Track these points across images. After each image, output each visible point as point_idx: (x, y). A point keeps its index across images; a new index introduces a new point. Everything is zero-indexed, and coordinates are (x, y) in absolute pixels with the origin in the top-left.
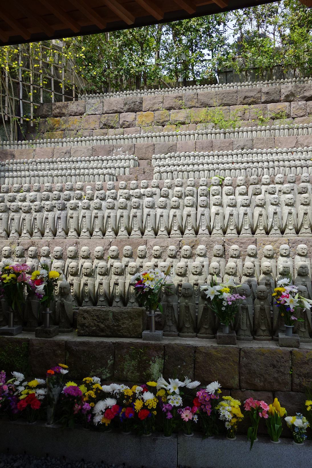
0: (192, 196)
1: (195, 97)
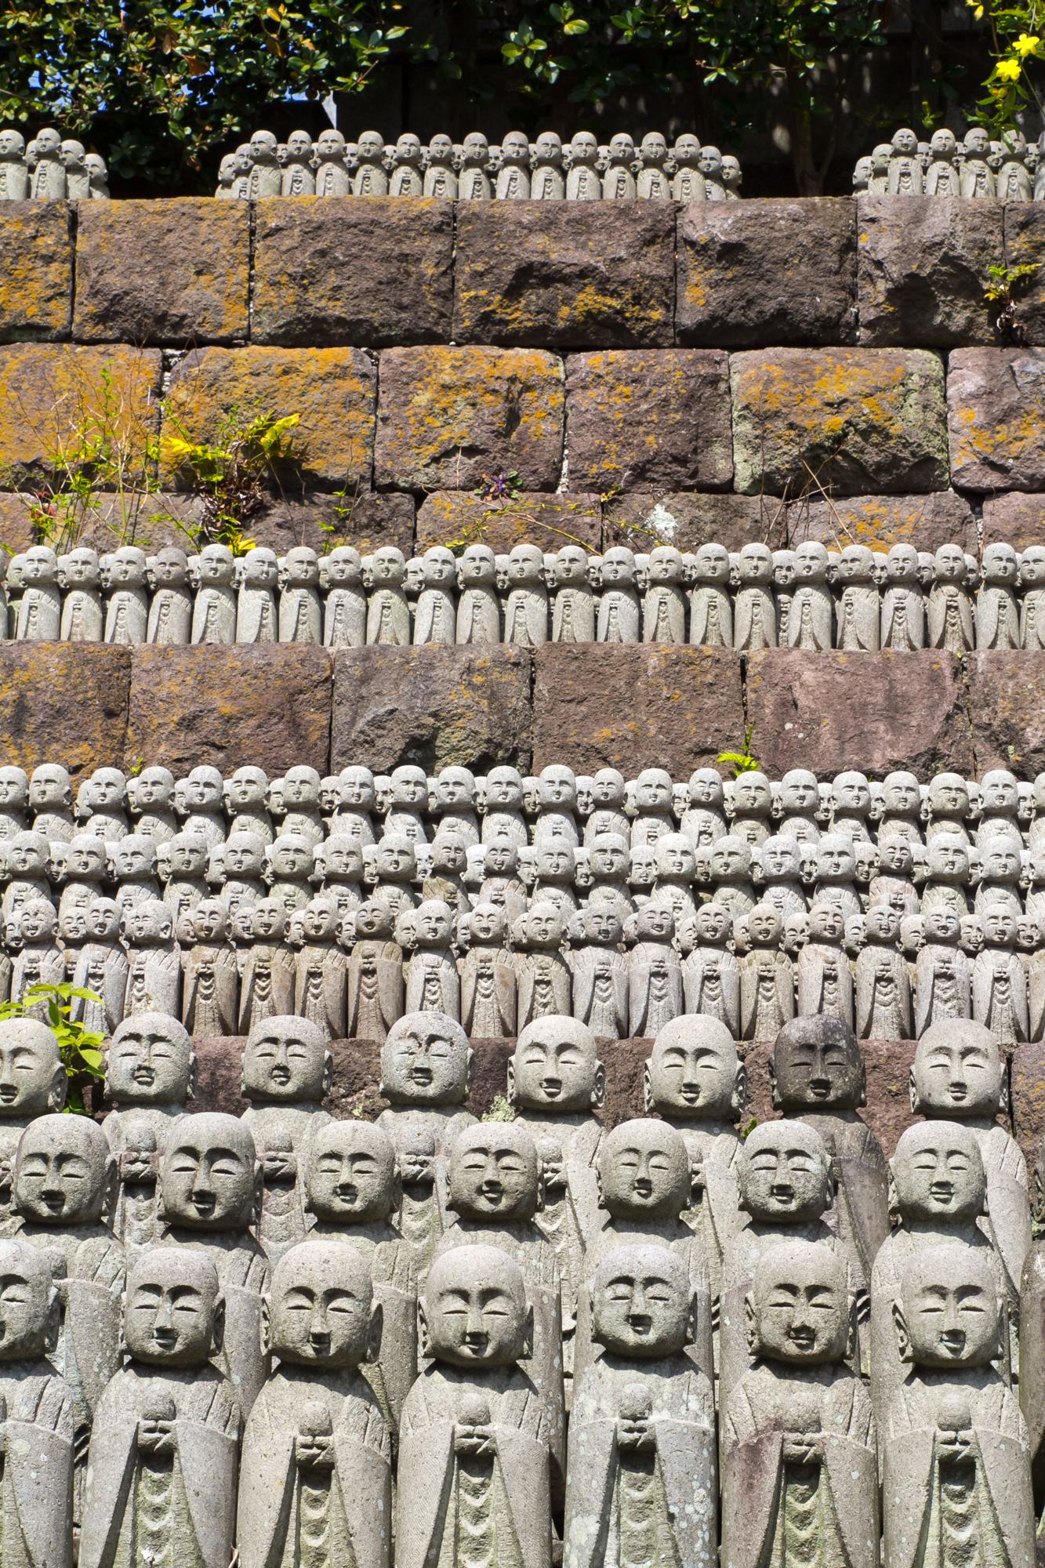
0: (965, 1222)
1: (47, 243)
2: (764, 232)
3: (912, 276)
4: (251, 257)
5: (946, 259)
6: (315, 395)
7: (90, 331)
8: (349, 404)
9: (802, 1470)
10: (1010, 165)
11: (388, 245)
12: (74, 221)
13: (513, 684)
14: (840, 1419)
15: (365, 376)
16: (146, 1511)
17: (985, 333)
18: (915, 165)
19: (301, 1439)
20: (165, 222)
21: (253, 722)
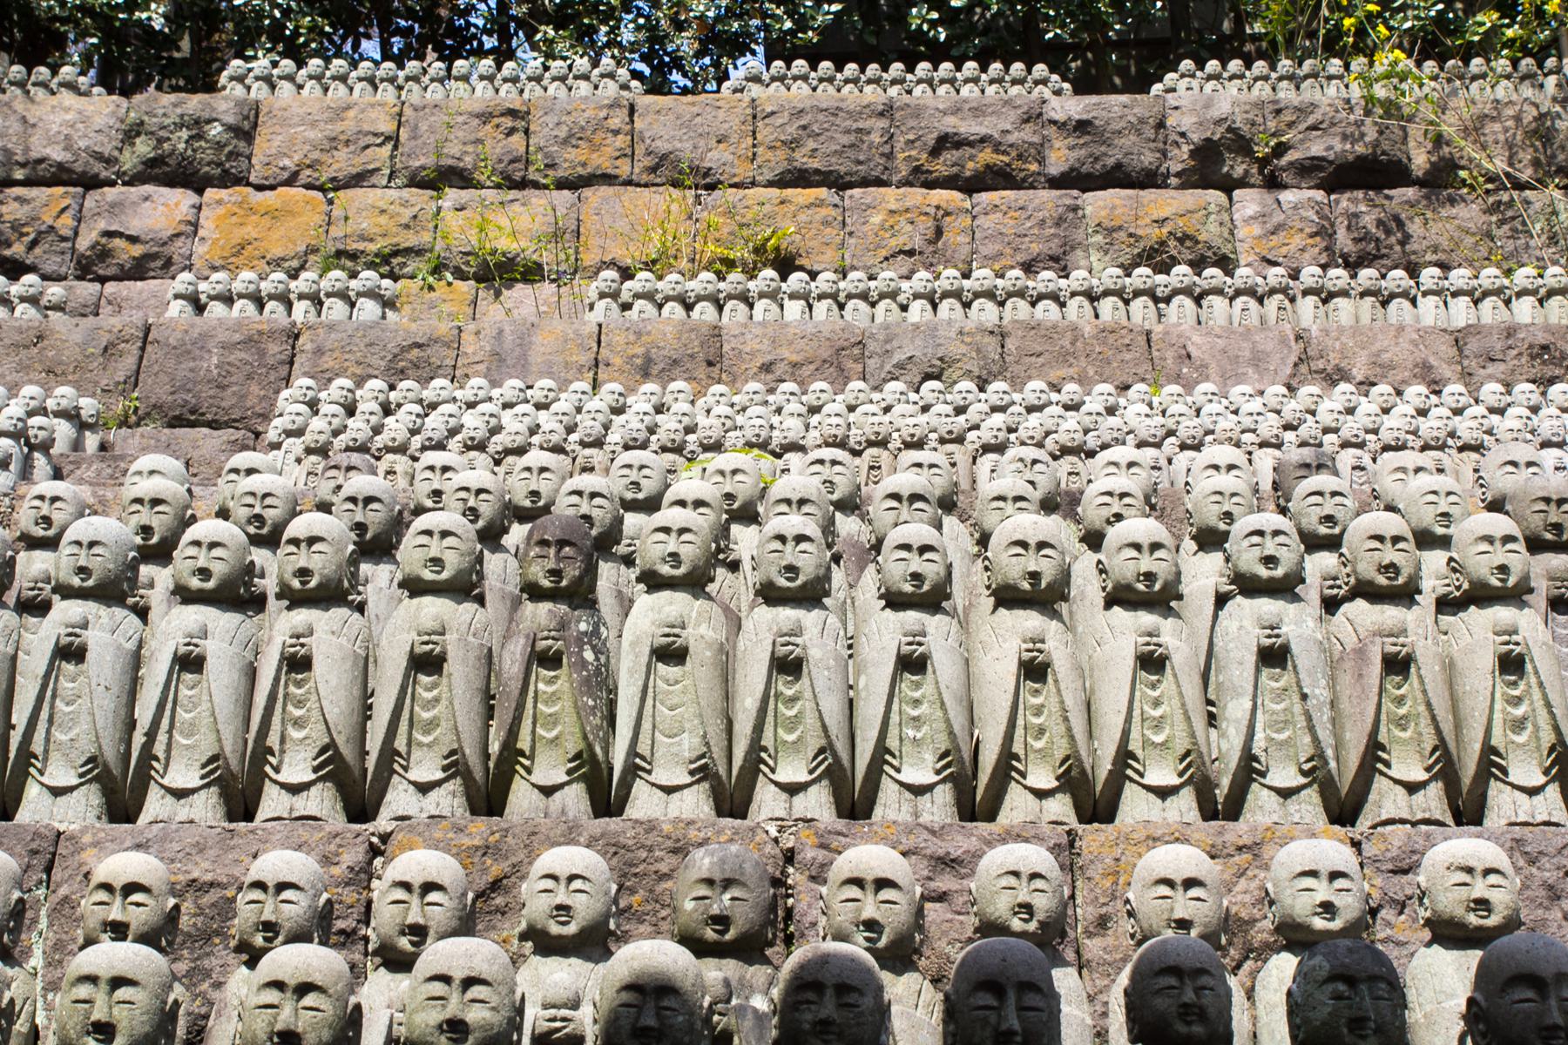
2: (1104, 113)
3: (1208, 140)
4: (754, 132)
5: (1229, 130)
6: (802, 217)
7: (645, 178)
8: (826, 223)
9: (1397, 665)
10: (1259, 83)
11: (848, 123)
12: (632, 110)
13: (991, 344)
14: (1420, 631)
15: (836, 206)
16: (907, 703)
17: (1256, 179)
18: (1195, 83)
19: (1024, 646)
20: (695, 110)
21: (812, 367)
